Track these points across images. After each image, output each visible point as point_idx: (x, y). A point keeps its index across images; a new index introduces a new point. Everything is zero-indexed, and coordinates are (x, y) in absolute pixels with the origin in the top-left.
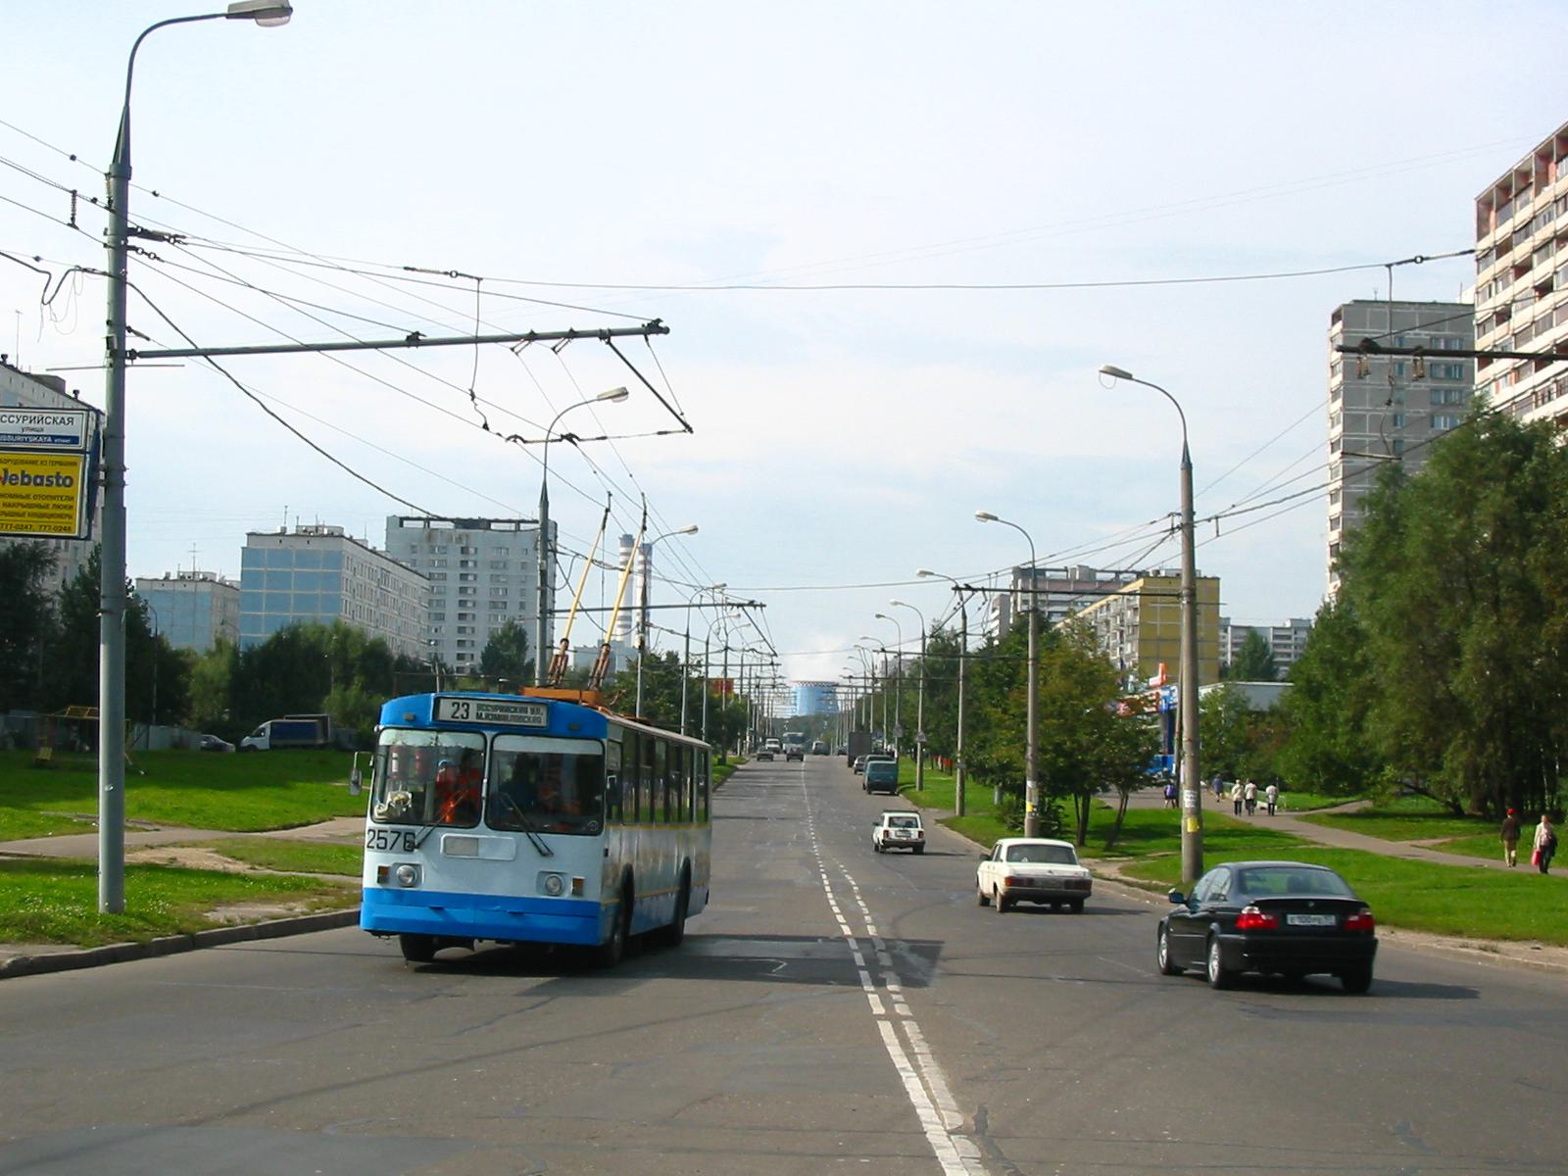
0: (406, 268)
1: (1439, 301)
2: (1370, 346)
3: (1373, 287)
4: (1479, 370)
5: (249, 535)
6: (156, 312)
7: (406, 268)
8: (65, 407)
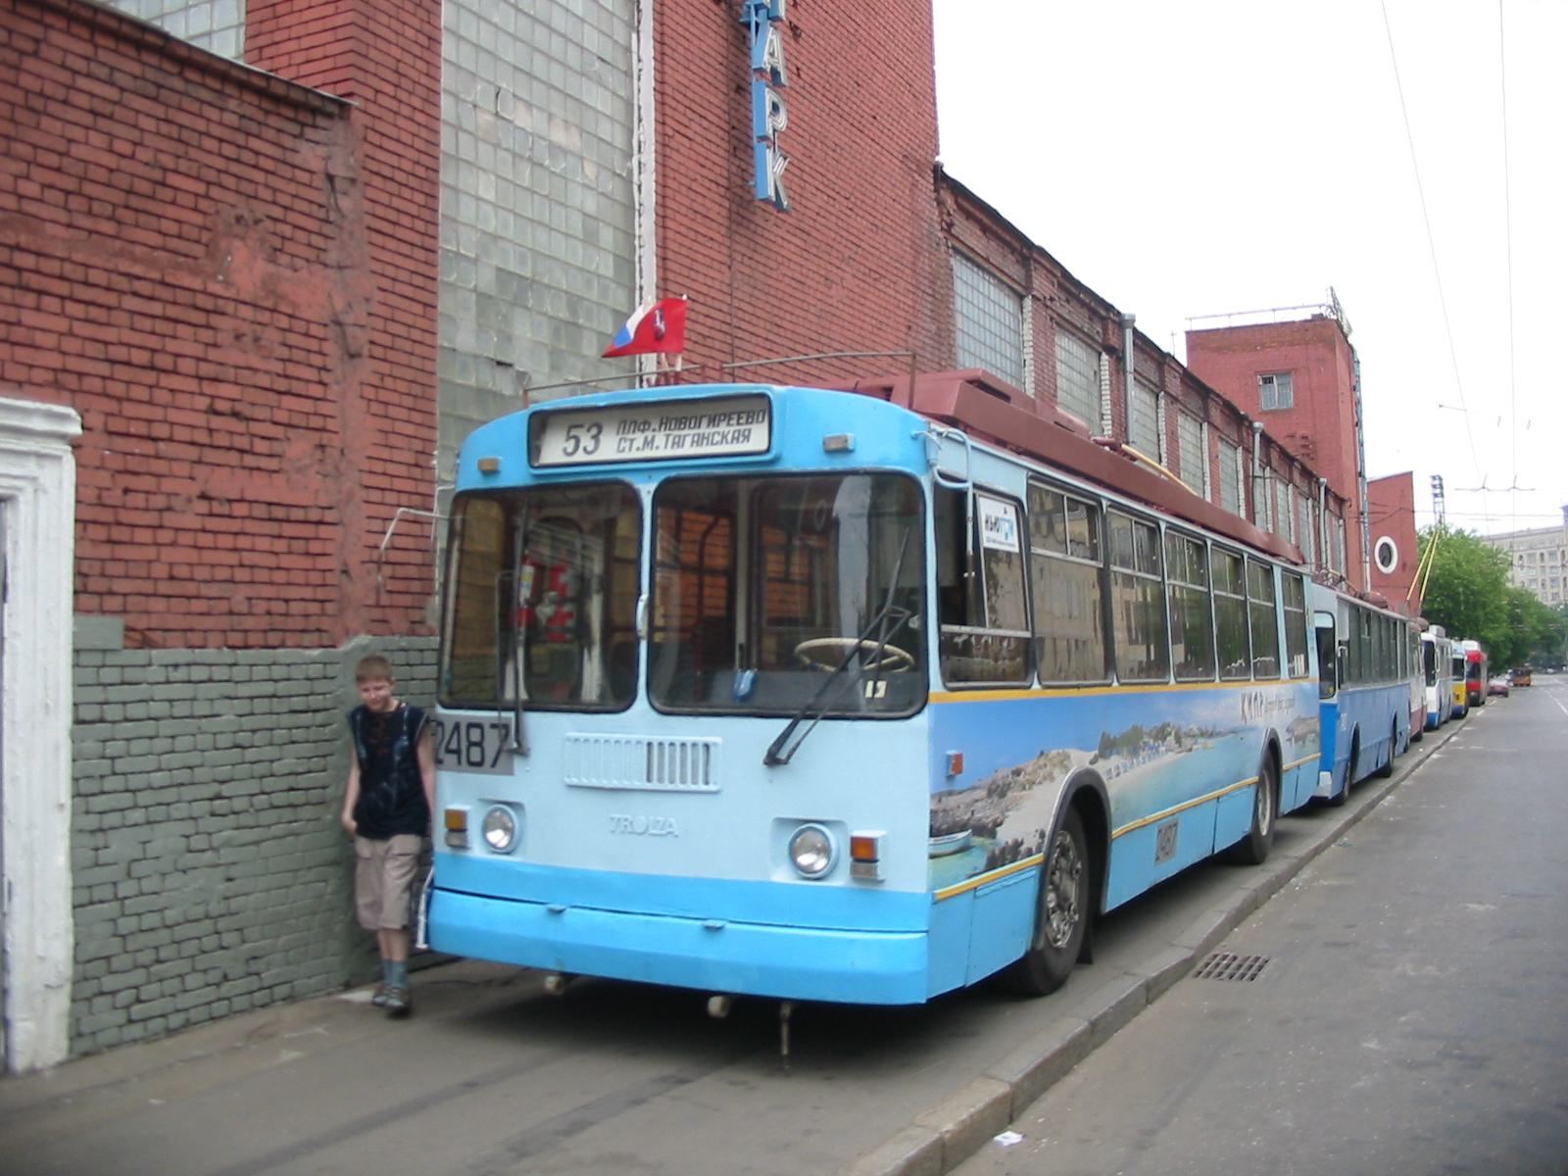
6: (259, 391)
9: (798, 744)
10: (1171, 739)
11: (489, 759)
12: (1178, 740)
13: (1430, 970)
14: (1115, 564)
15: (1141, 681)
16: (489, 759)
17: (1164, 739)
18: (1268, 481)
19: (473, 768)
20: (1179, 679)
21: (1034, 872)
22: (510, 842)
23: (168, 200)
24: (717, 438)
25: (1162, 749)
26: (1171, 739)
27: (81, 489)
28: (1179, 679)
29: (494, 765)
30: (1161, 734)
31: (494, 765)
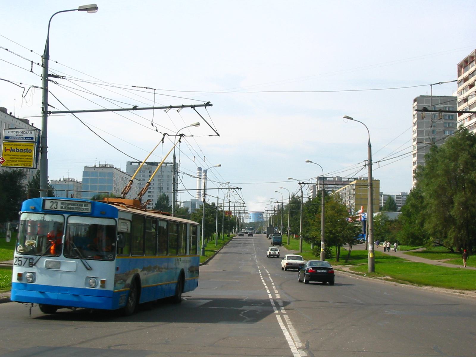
0: (133, 86)
1: (446, 96)
2: (425, 110)
3: (426, 91)
4: (458, 117)
5: (85, 167)
6: (152, 150)
7: (133, 86)
8: (29, 128)
9: (89, 266)
10: (157, 269)
11: (23, 264)
12: (159, 269)
13: (268, 338)
14: (170, 232)
15: (150, 255)
16: (23, 264)
17: (156, 269)
18: (244, 211)
19: (30, 267)
20: (133, 255)
21: (125, 294)
22: (32, 280)
23: (163, 136)
24: (67, 208)
25: (155, 271)
26: (157, 269)
27: (175, 216)
28: (133, 255)
29: (24, 265)
30: (155, 268)
31: (24, 265)
